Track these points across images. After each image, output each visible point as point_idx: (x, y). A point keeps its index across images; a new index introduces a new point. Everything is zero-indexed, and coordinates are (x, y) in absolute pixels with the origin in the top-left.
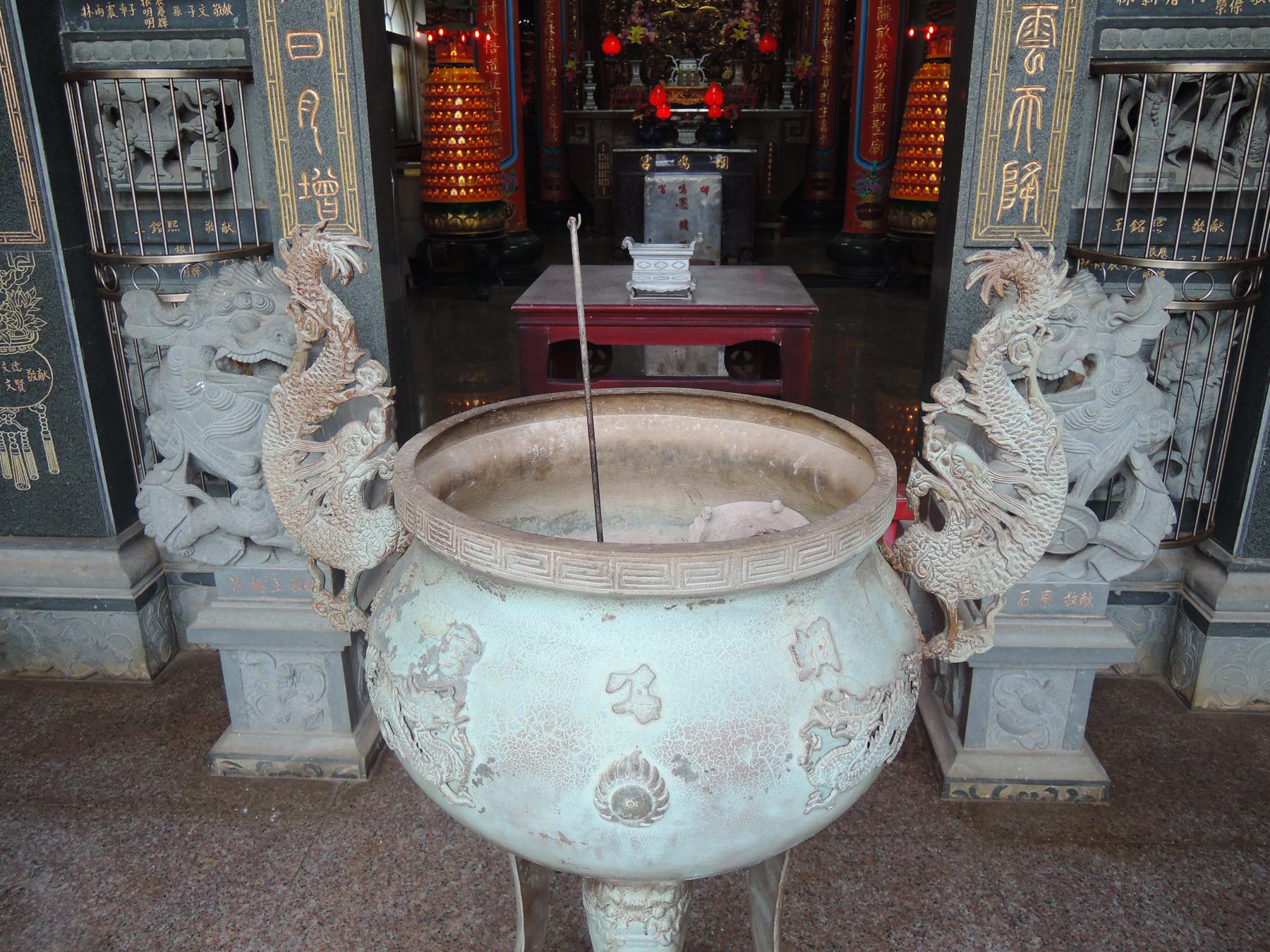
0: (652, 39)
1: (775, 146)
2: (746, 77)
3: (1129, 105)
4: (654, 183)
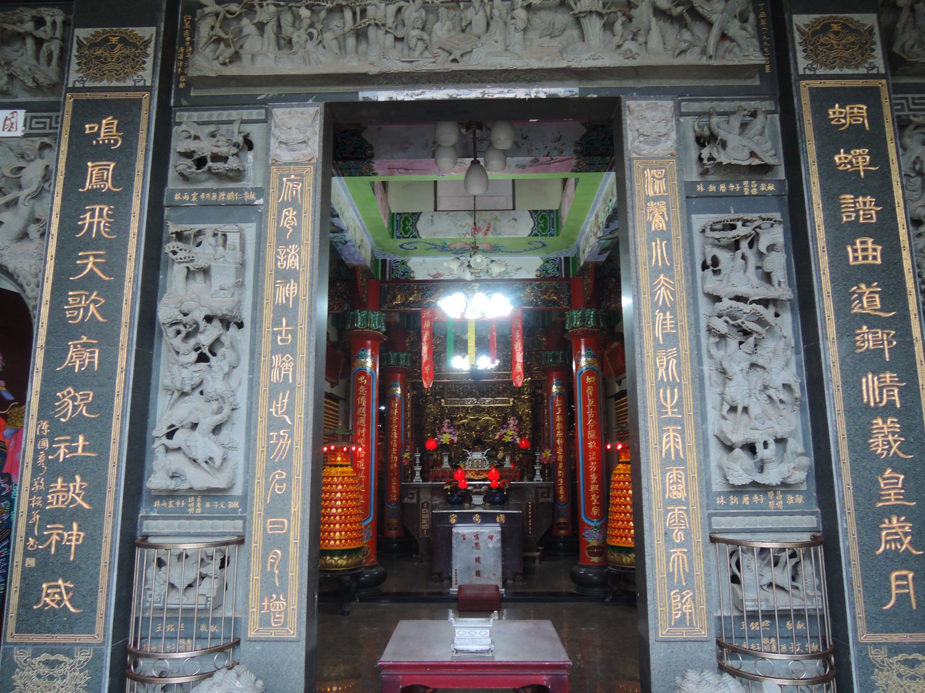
0: (455, 441)
1: (532, 504)
2: (512, 461)
3: (734, 559)
4: (458, 533)
